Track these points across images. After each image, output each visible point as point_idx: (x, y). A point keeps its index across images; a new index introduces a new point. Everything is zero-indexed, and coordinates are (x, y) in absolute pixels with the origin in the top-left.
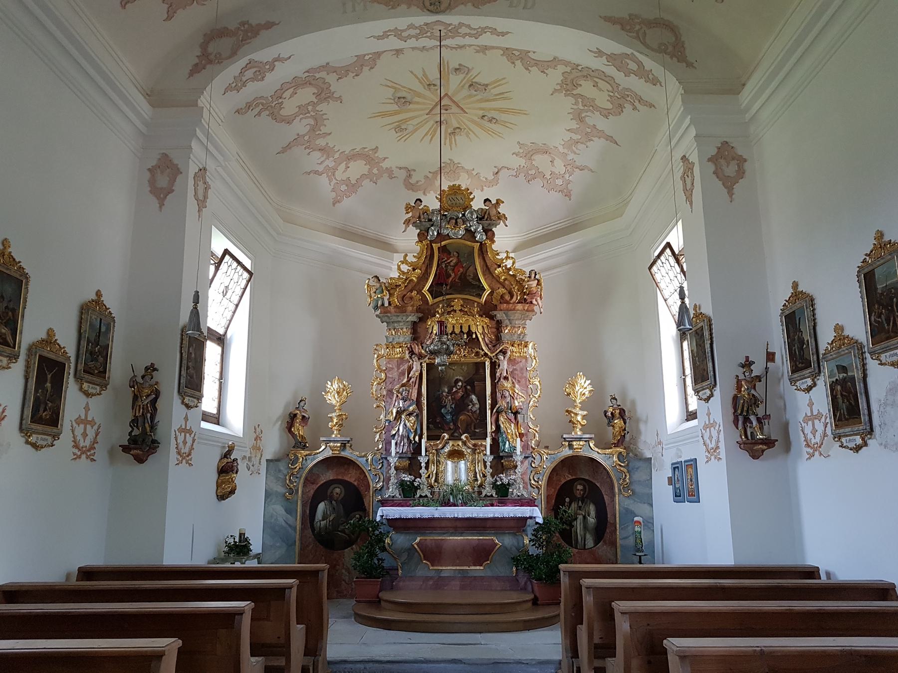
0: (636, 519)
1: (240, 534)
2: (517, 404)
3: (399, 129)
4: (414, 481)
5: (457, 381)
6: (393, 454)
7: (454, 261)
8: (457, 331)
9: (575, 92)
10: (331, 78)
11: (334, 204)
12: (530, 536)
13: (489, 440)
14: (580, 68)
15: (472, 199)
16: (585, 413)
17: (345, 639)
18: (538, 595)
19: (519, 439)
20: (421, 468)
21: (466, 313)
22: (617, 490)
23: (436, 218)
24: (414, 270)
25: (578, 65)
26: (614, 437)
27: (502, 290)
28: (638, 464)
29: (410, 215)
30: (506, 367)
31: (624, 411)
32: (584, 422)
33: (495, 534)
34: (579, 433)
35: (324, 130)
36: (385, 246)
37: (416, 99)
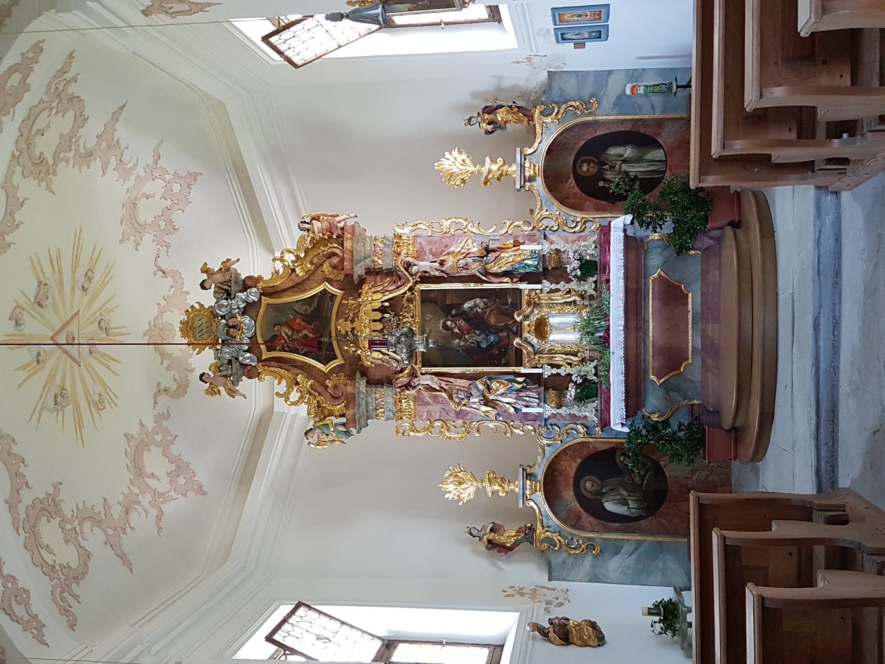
0: (628, 92)
1: (650, 614)
2: (476, 249)
3: (99, 405)
4: (575, 383)
5: (445, 327)
6: (540, 410)
7: (285, 331)
8: (379, 326)
9: (51, 161)
10: (27, 497)
11: (205, 493)
12: (649, 232)
13: (523, 286)
14: (17, 153)
15: (201, 305)
16: (488, 159)
17: (787, 468)
18: (726, 222)
19: (522, 247)
20: (559, 374)
21: (356, 315)
22: (590, 118)
23: (227, 353)
24: (297, 383)
25: (13, 156)
26: (520, 121)
27: (326, 267)
28: (556, 86)
29: (222, 389)
30: (427, 263)
31: (486, 107)
32: (500, 161)
33: (646, 277)
34: (514, 167)
35: (99, 508)
36: (263, 425)
37: (58, 380)
